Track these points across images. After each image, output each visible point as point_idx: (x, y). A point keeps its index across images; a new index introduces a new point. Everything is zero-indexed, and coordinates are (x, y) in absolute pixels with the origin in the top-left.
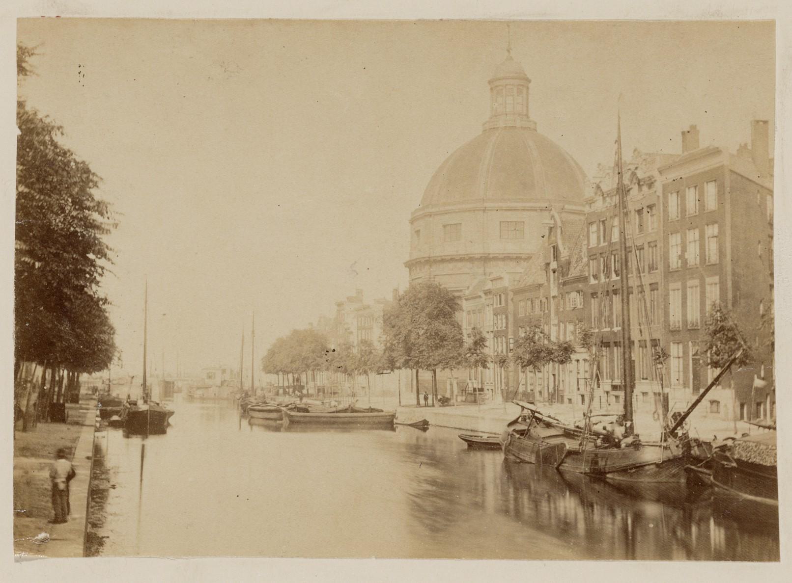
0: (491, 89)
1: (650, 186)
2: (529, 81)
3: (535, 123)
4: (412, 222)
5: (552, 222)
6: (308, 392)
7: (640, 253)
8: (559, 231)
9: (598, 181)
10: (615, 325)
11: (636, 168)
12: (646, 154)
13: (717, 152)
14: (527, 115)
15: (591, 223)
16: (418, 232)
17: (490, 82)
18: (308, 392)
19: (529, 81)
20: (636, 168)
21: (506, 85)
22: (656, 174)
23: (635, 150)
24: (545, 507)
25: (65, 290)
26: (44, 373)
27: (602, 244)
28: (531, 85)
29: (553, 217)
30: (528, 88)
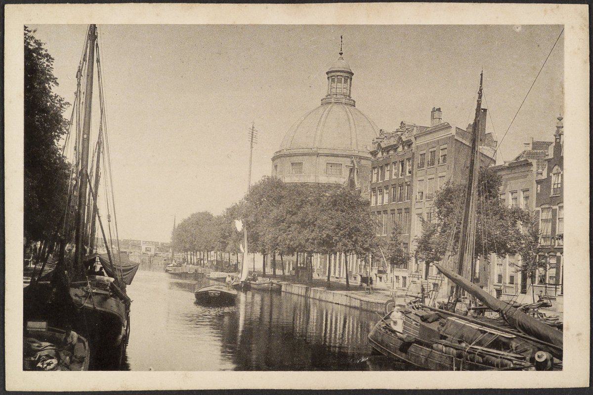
0: (328, 78)
1: (409, 146)
2: (353, 74)
3: (354, 102)
4: (273, 159)
5: (352, 165)
6: (347, 282)
7: (408, 188)
8: (356, 171)
9: (379, 141)
10: (383, 233)
11: (402, 134)
12: (409, 126)
13: (448, 127)
14: (349, 96)
15: (374, 168)
16: (276, 166)
17: (327, 73)
18: (347, 282)
19: (353, 74)
20: (402, 134)
21: (338, 76)
22: (413, 139)
23: (402, 123)
24: (50, 257)
25: (44, 324)
26: (262, 300)
27: (380, 181)
28: (353, 77)
29: (352, 162)
30: (351, 79)
